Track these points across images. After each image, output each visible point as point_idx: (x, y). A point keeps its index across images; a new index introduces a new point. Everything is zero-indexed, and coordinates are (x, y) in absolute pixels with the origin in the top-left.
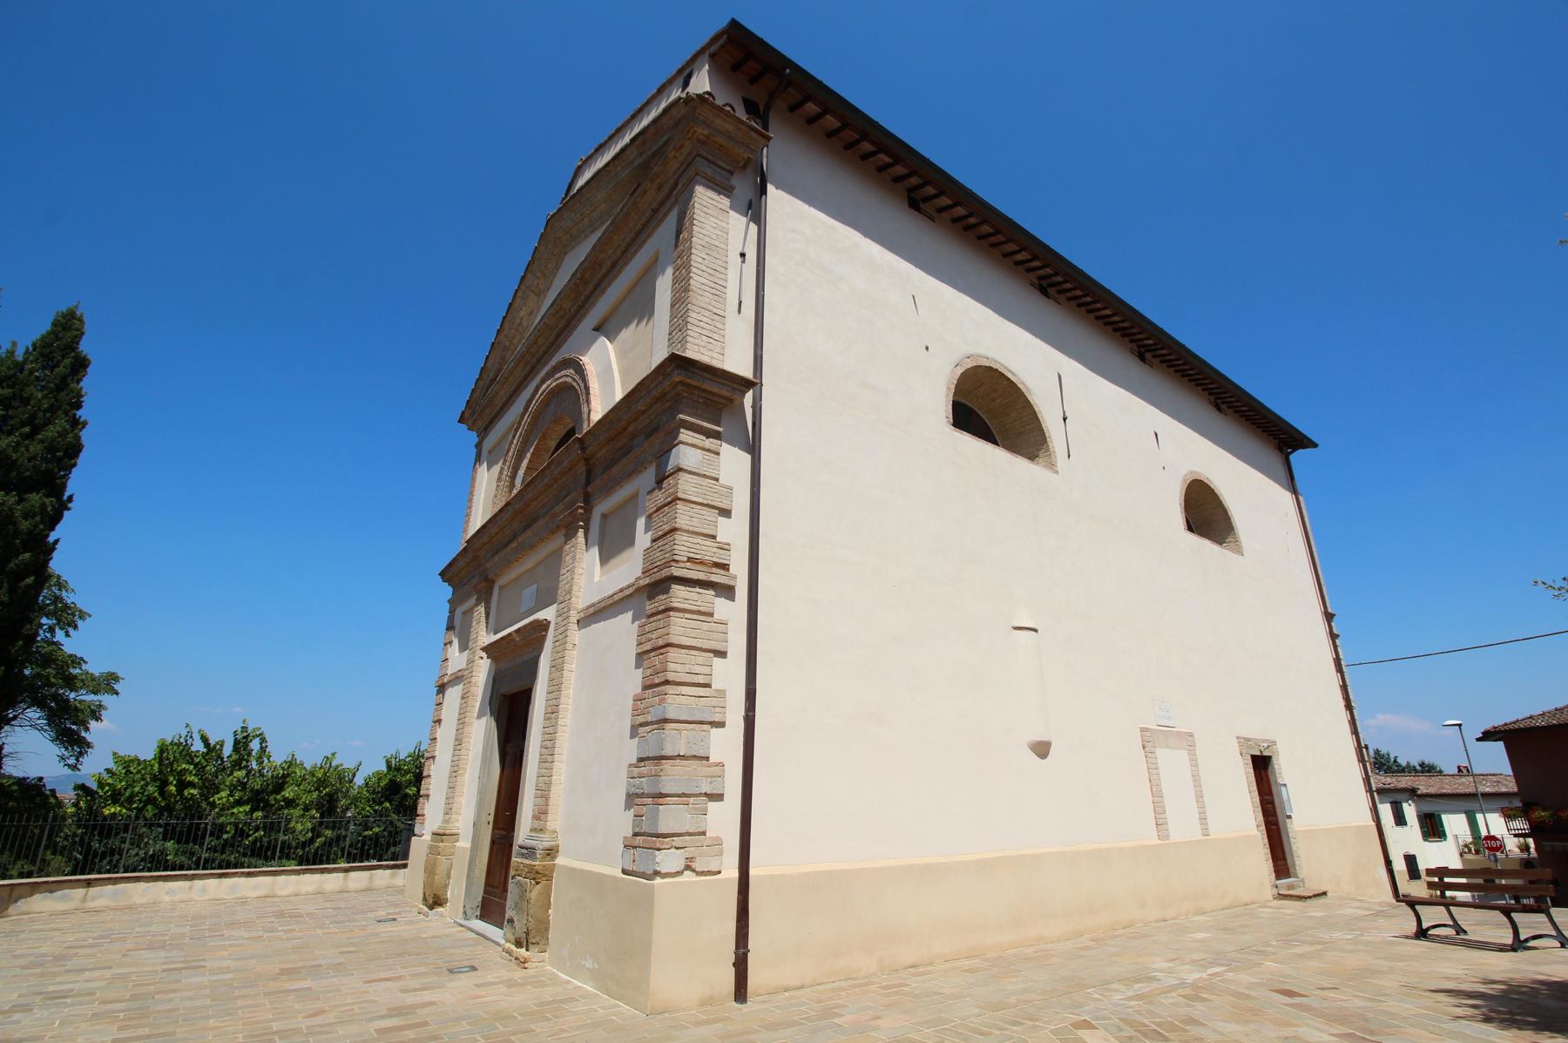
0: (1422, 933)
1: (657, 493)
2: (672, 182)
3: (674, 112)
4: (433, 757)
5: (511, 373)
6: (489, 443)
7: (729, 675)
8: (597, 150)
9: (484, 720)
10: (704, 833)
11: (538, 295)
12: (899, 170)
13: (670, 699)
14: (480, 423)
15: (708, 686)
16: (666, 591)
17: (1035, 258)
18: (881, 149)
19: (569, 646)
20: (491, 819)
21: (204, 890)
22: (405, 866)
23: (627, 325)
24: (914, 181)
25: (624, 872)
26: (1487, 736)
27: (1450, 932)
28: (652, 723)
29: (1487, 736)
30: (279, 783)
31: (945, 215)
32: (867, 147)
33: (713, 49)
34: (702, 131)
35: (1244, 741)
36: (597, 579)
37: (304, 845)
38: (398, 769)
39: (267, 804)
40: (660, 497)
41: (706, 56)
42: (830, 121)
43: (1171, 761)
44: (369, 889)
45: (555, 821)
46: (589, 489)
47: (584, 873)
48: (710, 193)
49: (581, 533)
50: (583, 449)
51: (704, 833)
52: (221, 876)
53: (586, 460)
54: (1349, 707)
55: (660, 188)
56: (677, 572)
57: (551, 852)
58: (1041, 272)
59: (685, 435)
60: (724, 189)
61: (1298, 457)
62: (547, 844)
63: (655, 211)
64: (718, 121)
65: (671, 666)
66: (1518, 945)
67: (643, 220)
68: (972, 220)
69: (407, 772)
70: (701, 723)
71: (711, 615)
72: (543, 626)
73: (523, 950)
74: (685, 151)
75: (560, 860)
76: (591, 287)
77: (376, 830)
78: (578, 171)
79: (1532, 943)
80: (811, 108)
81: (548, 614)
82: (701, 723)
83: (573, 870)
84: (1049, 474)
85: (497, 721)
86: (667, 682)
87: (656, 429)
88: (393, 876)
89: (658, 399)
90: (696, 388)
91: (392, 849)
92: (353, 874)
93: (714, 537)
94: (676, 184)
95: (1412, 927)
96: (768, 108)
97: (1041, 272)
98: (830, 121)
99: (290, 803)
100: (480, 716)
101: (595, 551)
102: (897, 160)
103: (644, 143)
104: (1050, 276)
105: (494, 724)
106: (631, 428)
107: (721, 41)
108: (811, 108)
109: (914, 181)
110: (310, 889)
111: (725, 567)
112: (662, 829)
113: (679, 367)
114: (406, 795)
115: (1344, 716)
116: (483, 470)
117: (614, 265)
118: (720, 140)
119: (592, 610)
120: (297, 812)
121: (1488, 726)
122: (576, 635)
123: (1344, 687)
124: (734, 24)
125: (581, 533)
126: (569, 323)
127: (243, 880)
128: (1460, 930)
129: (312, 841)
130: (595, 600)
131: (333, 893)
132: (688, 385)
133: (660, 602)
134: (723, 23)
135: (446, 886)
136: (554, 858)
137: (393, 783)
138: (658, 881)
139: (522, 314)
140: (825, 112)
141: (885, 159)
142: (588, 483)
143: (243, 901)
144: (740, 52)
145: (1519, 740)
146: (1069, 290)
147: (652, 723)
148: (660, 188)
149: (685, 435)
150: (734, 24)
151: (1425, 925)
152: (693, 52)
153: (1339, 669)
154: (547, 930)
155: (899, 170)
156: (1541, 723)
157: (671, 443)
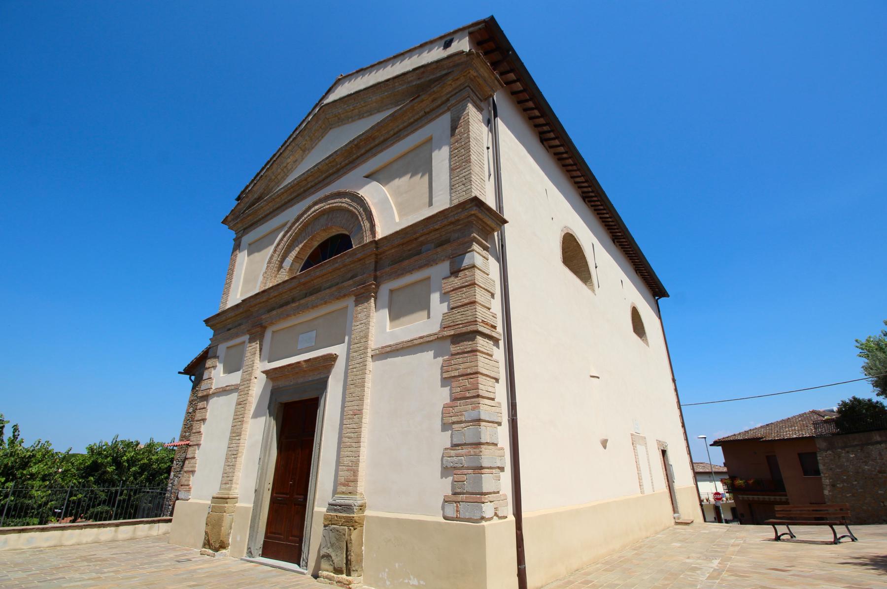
0: (778, 538)
1: (452, 279)
2: (444, 99)
3: (456, 58)
4: (198, 445)
5: (279, 196)
6: (246, 239)
7: (501, 391)
8: (357, 72)
9: (262, 420)
10: (498, 492)
11: (304, 151)
12: (541, 121)
13: (482, 407)
14: (239, 225)
15: (493, 399)
16: (473, 339)
17: (586, 181)
18: (537, 108)
19: (367, 372)
20: (270, 486)
21: (6, 542)
22: (170, 521)
23: (400, 175)
24: (545, 128)
25: (445, 518)
26: (716, 443)
27: (788, 537)
28: (466, 422)
29: (716, 443)
30: (25, 462)
31: (553, 150)
32: (531, 104)
33: (471, 29)
34: (473, 73)
35: (659, 442)
36: (388, 330)
37: (40, 506)
38: (100, 454)
39: (15, 477)
40: (456, 282)
41: (467, 31)
42: (518, 86)
43: (640, 449)
44: (113, 541)
45: (363, 486)
46: (378, 273)
47: (399, 521)
48: (474, 109)
49: (372, 300)
50: (377, 248)
51: (498, 492)
52: (20, 531)
53: (376, 255)
54: (683, 426)
55: (434, 100)
56: (481, 329)
57: (362, 508)
58: (585, 190)
59: (475, 246)
60: (480, 109)
61: (662, 301)
62: (360, 503)
63: (426, 113)
64: (482, 70)
65: (480, 386)
66: (836, 541)
67: (417, 117)
68: (565, 156)
69: (106, 457)
70: (493, 422)
71: (491, 356)
72: (331, 359)
73: (344, 576)
74: (459, 83)
75: (367, 513)
76: (363, 151)
77: (80, 496)
78: (338, 82)
79: (842, 540)
80: (512, 76)
81: (339, 350)
82: (493, 422)
83: (411, 521)
84: (590, 292)
85: (276, 419)
86: (478, 396)
87: (447, 241)
88: (150, 529)
89: (451, 223)
90: (481, 220)
91: (91, 510)
92: (122, 528)
93: (489, 309)
94: (448, 100)
95: (773, 536)
96: (495, 71)
97: (585, 190)
98: (518, 86)
99: (33, 476)
100: (256, 415)
101: (385, 312)
102: (543, 115)
103: (423, 72)
104: (589, 192)
105: (273, 423)
106: (421, 239)
107: (480, 26)
108: (512, 76)
109: (545, 128)
110: (90, 539)
111: (495, 327)
112: (484, 491)
113: (476, 205)
114: (106, 472)
115: (681, 430)
116: (243, 257)
117: (385, 140)
118: (481, 81)
119: (388, 349)
120: (37, 483)
121: (716, 439)
122: (371, 365)
123: (681, 415)
124: (492, 19)
125: (372, 300)
126: (338, 170)
127: (38, 534)
128: (793, 536)
129: (46, 504)
130: (391, 343)
131: (124, 540)
132: (477, 217)
133: (466, 345)
134: (485, 16)
135: (229, 534)
136: (363, 512)
137: (95, 463)
138: (484, 523)
139: (289, 160)
140: (518, 80)
141: (537, 113)
142: (376, 270)
143: (40, 550)
144: (489, 37)
145: (728, 445)
146: (595, 201)
147: (466, 422)
148: (433, 101)
149: (475, 246)
150: (492, 19)
151: (838, 536)
152: (456, 28)
153: (680, 408)
154: (361, 561)
155: (541, 121)
156: (739, 438)
157: (466, 249)
